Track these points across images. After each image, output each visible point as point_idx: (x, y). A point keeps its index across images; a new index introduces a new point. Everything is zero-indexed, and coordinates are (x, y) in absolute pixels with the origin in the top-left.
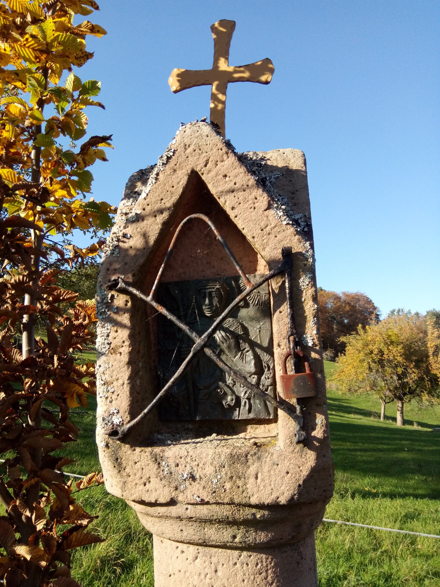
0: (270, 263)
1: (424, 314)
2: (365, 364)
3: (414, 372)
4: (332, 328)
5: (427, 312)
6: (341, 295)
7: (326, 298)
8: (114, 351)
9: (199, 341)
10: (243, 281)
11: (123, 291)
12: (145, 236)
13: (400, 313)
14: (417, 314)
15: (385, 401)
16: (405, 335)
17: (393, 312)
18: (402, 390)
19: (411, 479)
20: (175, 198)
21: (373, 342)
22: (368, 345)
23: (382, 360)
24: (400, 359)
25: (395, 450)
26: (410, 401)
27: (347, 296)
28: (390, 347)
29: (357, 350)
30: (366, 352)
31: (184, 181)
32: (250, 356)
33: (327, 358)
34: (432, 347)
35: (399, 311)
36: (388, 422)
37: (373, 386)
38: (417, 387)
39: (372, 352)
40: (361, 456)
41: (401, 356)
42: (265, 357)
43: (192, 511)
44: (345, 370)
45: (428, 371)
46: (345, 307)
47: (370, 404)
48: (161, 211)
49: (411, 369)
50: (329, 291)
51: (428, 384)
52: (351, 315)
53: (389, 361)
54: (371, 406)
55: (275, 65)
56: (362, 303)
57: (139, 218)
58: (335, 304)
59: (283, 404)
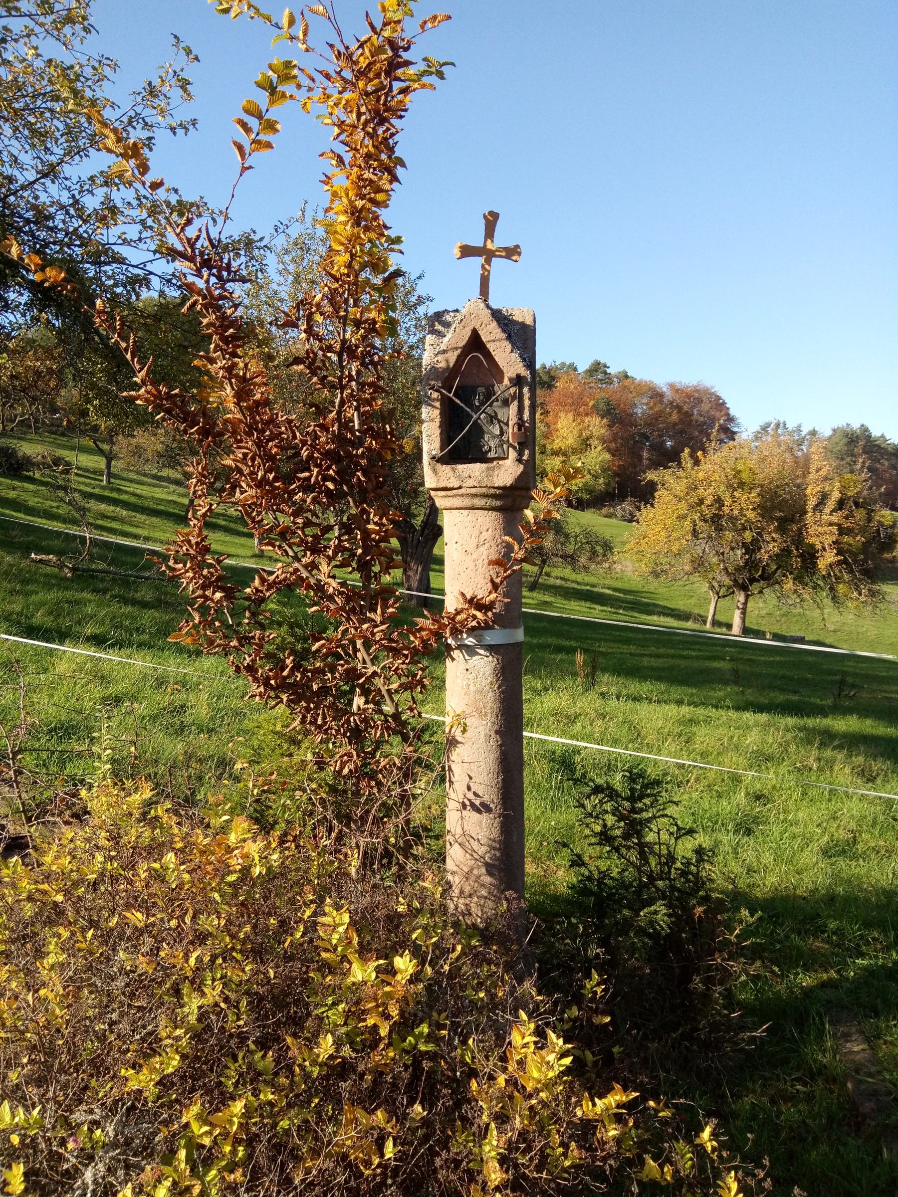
0: (510, 380)
1: (828, 433)
2: (687, 523)
3: (774, 540)
4: (640, 458)
5: (834, 430)
6: (665, 389)
7: (634, 394)
8: (432, 420)
9: (475, 416)
10: (496, 388)
11: (437, 391)
12: (447, 361)
13: (780, 431)
14: (813, 433)
15: (718, 593)
16: (768, 473)
17: (765, 428)
18: (750, 571)
19: (720, 690)
20: (464, 342)
21: (707, 481)
22: (696, 488)
23: (720, 517)
24: (751, 515)
25: (710, 658)
26: (761, 592)
27: (677, 391)
28: (736, 494)
29: (676, 496)
30: (691, 501)
31: (469, 334)
32: (497, 426)
33: (623, 516)
34: (813, 496)
35: (778, 425)
36: (718, 630)
37: (699, 564)
38: (777, 569)
39: (701, 502)
40: (646, 662)
41: (754, 509)
42: (505, 427)
43: (469, 491)
44: (650, 533)
45: (799, 540)
46: (670, 414)
47: (693, 601)
48: (456, 349)
49: (770, 533)
50: (641, 381)
51: (796, 562)
52: (682, 432)
53: (733, 519)
54: (695, 605)
55: (523, 249)
56: (705, 407)
57: (444, 352)
58: (651, 408)
59: (511, 445)
